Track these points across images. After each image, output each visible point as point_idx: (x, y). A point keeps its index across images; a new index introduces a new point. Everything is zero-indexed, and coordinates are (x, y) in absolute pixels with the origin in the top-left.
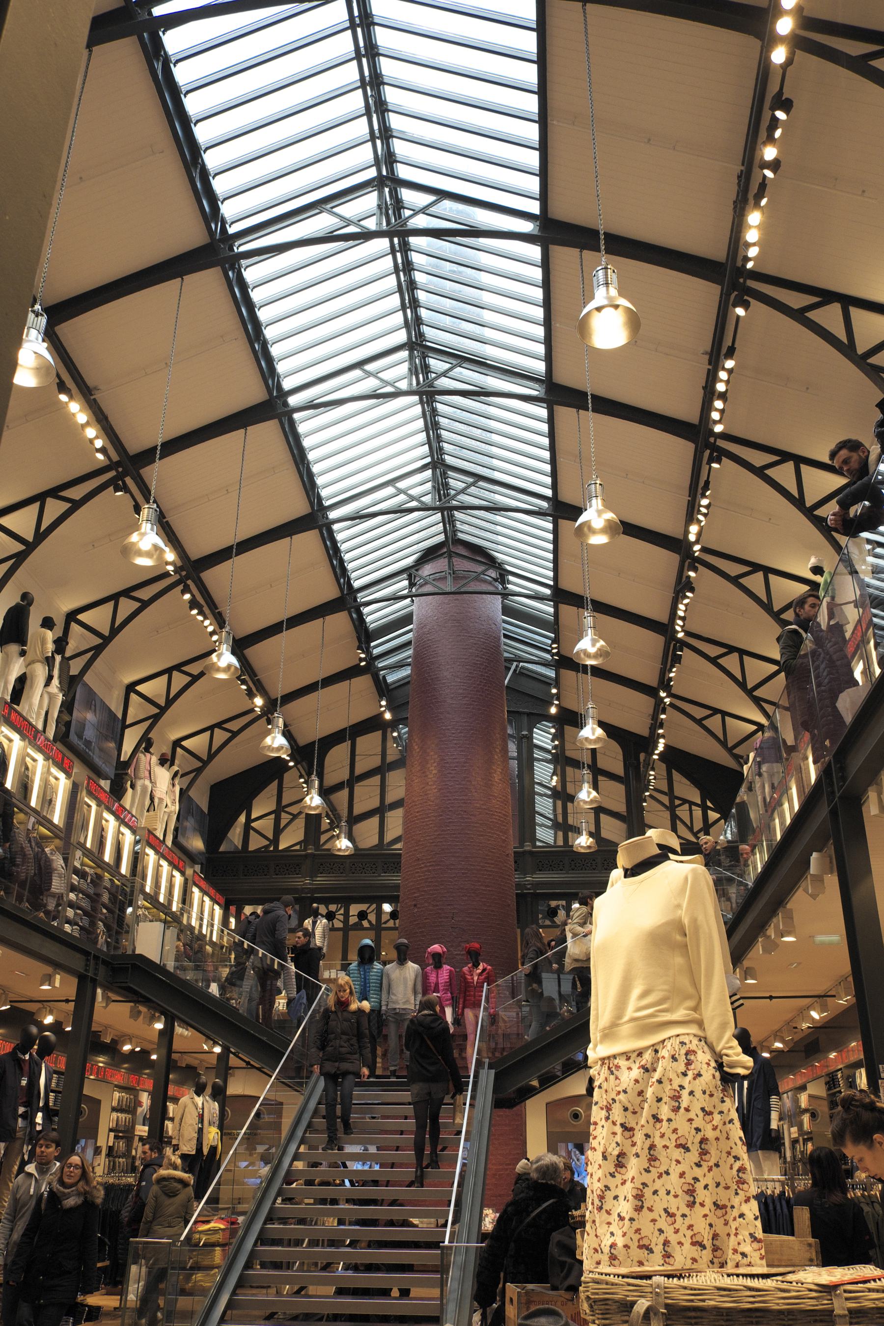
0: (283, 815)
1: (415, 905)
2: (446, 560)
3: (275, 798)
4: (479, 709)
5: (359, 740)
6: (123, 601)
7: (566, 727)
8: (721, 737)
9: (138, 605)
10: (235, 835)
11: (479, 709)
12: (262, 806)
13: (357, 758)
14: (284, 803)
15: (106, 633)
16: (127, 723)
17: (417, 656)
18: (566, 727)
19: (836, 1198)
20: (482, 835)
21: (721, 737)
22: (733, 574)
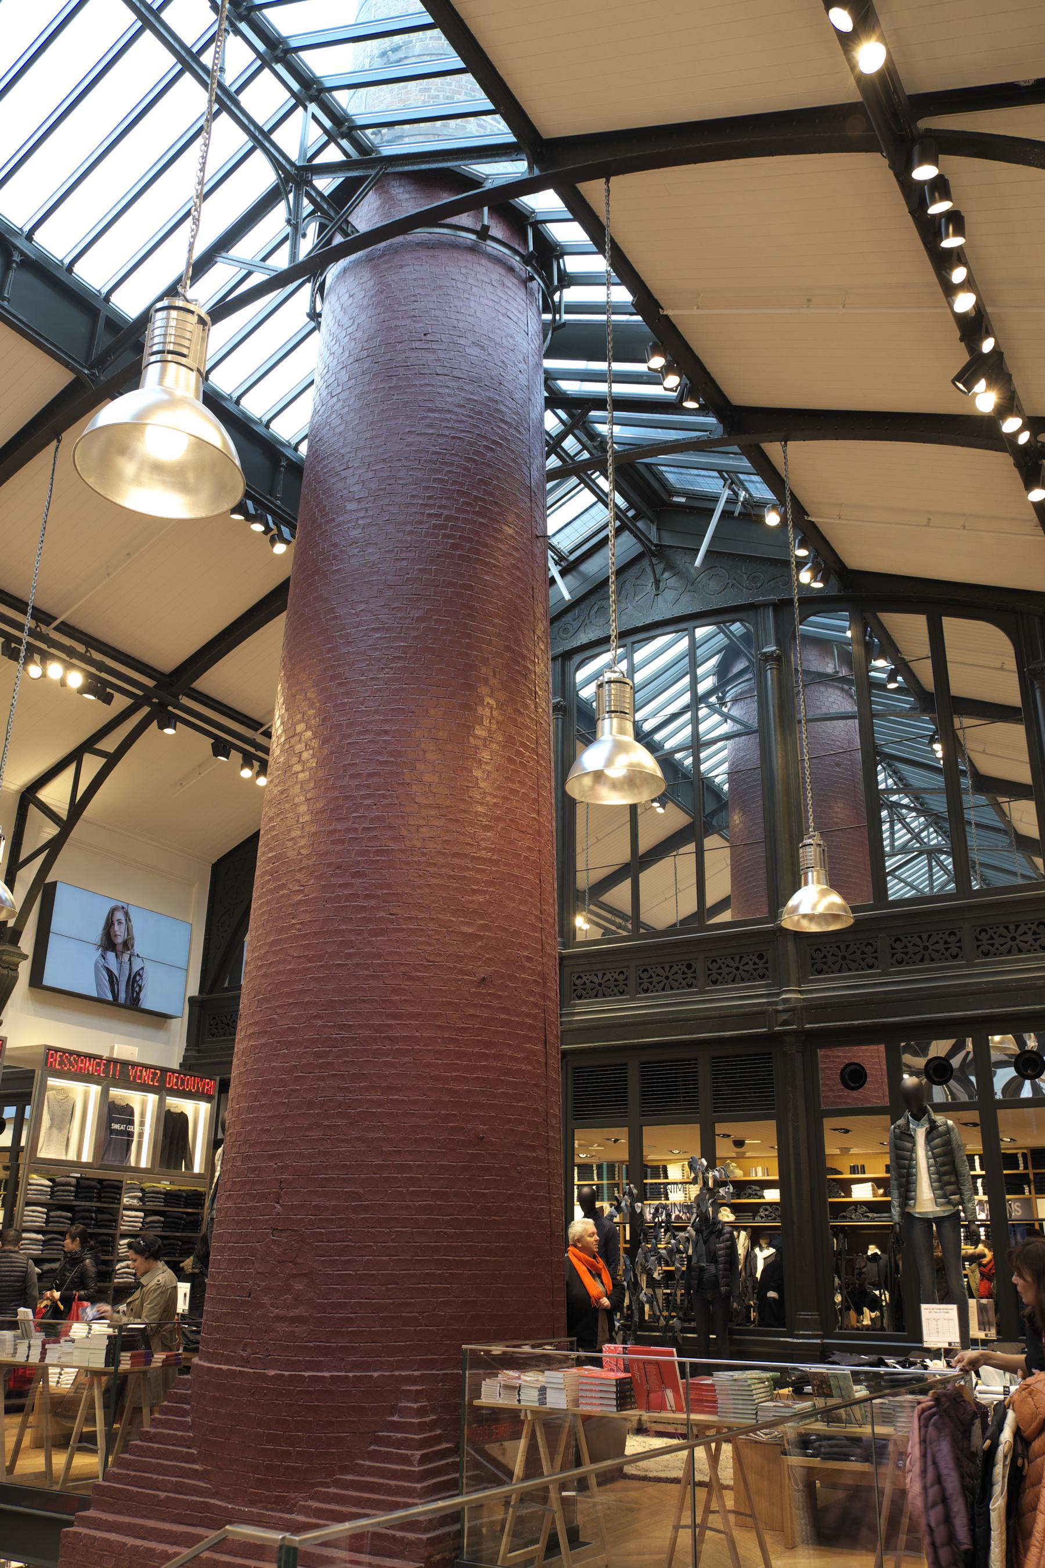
20: (382, 932)
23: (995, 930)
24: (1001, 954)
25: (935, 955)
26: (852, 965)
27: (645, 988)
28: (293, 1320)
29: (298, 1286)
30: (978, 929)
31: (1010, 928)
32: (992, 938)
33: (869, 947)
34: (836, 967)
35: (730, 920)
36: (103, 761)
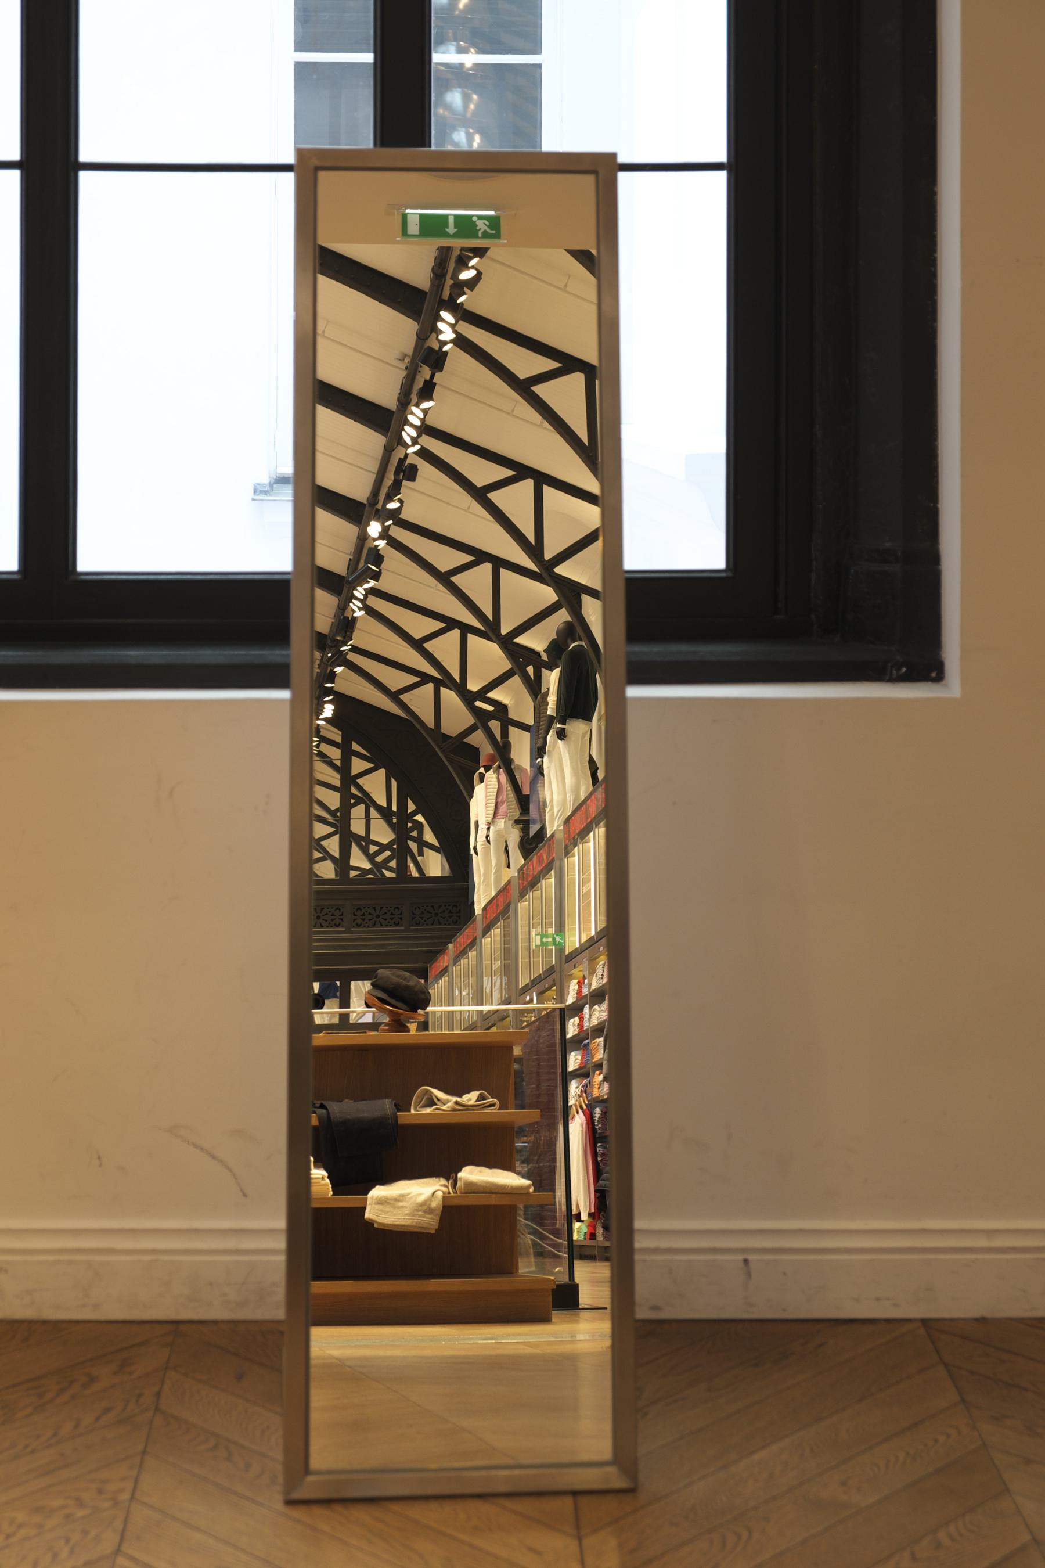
23: (366, 909)
24: (391, 925)
25: (324, 923)
26: (324, 923)
27: (359, 923)
30: (356, 908)
31: (376, 909)
32: (423, 913)
33: (397, 910)
34: (371, 923)
35: (440, 875)
36: (470, 636)
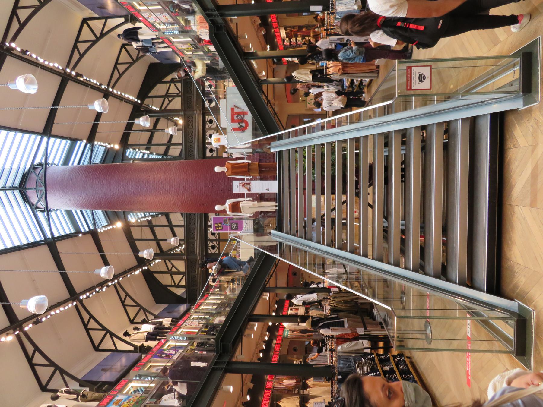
0: (172, 270)
1: (203, 205)
2: (27, 191)
3: (163, 274)
4: (109, 175)
5: (135, 237)
6: (35, 361)
7: (128, 143)
8: (128, 65)
9: (37, 353)
10: (180, 292)
11: (109, 175)
12: (165, 280)
13: (143, 238)
14: (167, 270)
15: (139, 308)
16: (115, 349)
17: (88, 207)
18: (128, 143)
19: (308, 314)
20: (170, 174)
21: (128, 65)
22: (78, 56)
28: (225, 182)
29: (220, 182)
